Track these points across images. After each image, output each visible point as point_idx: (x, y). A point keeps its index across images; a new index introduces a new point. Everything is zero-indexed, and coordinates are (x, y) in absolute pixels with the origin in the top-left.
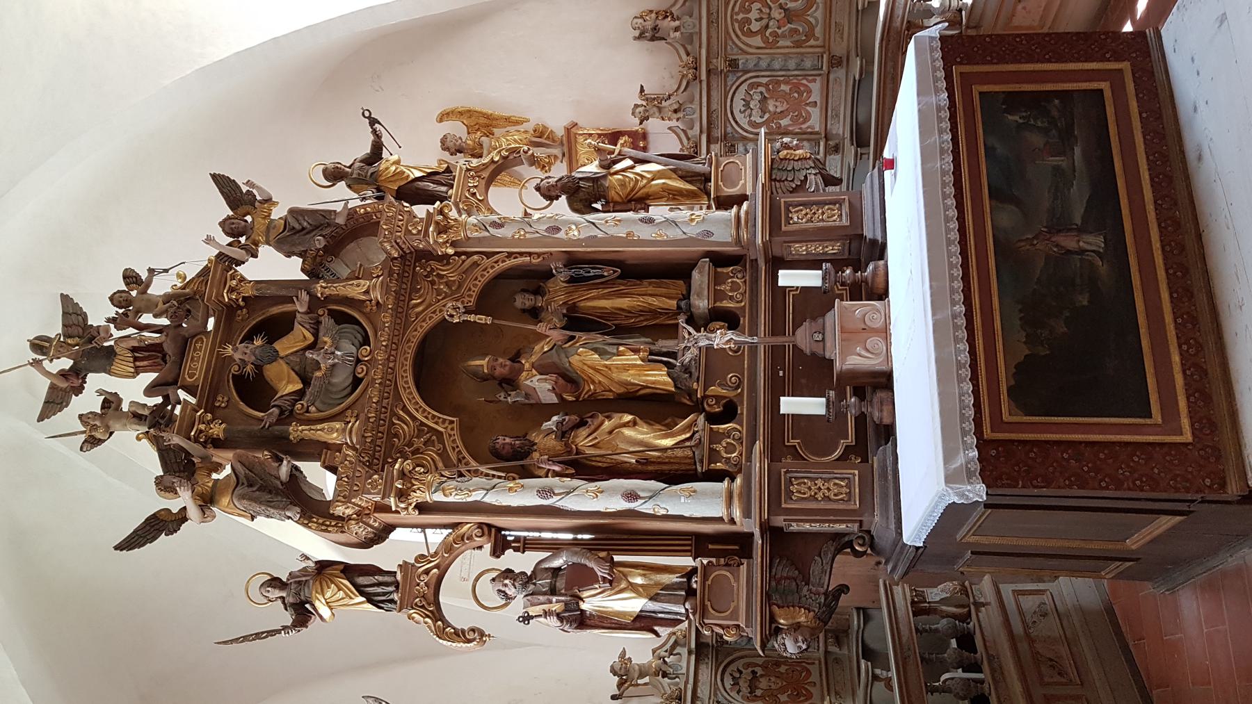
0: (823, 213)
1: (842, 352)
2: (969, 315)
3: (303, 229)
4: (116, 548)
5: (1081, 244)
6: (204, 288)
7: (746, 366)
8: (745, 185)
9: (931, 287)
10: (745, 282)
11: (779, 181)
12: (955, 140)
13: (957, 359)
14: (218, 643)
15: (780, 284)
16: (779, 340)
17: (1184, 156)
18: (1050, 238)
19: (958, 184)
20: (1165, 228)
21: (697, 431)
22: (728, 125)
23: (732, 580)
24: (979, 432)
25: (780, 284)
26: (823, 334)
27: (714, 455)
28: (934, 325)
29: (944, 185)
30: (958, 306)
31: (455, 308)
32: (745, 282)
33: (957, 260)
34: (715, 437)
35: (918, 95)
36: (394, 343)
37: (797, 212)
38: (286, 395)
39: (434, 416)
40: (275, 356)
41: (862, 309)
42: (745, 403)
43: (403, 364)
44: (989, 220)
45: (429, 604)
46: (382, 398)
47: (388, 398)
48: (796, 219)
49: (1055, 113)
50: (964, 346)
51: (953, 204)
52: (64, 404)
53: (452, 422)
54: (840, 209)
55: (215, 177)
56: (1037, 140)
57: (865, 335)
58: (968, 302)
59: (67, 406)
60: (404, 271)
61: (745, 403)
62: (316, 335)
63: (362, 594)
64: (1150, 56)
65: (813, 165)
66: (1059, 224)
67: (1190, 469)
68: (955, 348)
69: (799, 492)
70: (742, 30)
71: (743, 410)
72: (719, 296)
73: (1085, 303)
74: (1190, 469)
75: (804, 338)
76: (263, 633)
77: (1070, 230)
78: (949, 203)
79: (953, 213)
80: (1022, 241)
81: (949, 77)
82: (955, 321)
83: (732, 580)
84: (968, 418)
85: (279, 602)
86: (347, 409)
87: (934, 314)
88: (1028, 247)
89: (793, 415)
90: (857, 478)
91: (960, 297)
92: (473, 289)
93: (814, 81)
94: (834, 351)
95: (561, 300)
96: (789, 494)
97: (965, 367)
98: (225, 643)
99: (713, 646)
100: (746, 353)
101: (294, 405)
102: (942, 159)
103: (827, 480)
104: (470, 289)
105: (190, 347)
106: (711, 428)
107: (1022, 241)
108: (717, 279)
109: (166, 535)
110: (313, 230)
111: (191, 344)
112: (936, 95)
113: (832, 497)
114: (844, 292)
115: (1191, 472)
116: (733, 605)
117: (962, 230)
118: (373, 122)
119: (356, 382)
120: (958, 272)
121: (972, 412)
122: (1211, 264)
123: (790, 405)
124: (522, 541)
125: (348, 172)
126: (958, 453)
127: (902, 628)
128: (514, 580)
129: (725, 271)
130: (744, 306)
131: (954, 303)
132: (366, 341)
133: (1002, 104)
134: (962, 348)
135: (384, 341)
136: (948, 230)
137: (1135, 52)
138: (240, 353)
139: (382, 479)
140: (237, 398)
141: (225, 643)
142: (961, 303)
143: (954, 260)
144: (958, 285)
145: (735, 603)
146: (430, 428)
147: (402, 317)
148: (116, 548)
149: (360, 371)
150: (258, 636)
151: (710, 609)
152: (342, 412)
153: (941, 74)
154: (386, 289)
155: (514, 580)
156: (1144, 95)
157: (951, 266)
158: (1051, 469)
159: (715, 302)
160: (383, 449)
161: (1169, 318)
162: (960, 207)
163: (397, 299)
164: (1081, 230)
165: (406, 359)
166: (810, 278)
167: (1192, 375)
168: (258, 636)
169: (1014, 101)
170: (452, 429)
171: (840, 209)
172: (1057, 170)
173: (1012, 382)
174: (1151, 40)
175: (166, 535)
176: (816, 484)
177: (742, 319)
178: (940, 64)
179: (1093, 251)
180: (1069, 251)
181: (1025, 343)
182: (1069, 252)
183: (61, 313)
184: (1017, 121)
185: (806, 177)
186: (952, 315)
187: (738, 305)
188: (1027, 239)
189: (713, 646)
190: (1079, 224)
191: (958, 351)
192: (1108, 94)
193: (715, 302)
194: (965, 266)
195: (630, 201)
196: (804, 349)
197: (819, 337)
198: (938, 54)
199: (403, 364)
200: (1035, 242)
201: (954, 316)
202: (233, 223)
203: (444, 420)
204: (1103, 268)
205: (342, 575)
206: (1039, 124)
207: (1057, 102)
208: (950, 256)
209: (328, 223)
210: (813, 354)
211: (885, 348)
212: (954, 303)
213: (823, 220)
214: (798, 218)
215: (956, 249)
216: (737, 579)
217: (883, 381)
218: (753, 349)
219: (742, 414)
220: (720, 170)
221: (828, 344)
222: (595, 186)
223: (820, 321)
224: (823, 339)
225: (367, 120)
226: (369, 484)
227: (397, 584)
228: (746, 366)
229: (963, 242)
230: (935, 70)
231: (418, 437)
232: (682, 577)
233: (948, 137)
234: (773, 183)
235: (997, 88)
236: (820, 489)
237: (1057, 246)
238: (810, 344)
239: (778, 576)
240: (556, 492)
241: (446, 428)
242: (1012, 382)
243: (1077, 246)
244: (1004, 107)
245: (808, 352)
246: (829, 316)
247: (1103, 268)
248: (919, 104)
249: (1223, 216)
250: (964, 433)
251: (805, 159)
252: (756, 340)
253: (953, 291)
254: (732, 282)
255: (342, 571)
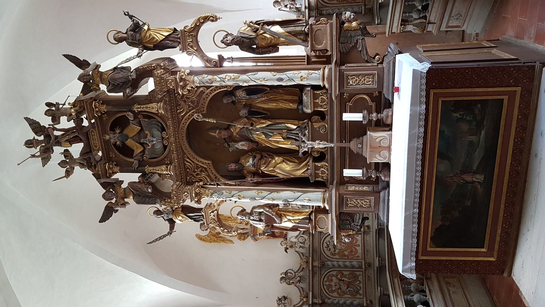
0: (365, 80)
1: (370, 157)
2: (420, 214)
3: (118, 84)
4: (101, 221)
5: (474, 179)
6: (83, 105)
7: (329, 138)
8: (326, 44)
9: (406, 201)
10: (328, 98)
11: (344, 43)
12: (425, 132)
13: (412, 230)
14: (148, 243)
15: (344, 119)
16: (343, 145)
17: (531, 143)
18: (461, 176)
19: (423, 154)
20: (517, 142)
21: (310, 169)
22: (322, 292)
23: (326, 219)
24: (417, 257)
25: (344, 119)
26: (362, 145)
27: (317, 175)
28: (405, 217)
29: (417, 154)
30: (416, 209)
31: (198, 116)
32: (328, 98)
33: (418, 190)
34: (317, 168)
35: (411, 105)
36: (176, 131)
37: (352, 79)
38: (139, 154)
39: (201, 161)
40: (127, 137)
41: (378, 135)
42: (329, 154)
43: (182, 139)
44: (435, 168)
45: (216, 222)
46: (178, 156)
47: (180, 154)
48: (351, 83)
49: (477, 112)
50: (416, 226)
51: (420, 164)
52: (49, 158)
53: (208, 164)
54: (373, 78)
55: (64, 55)
56: (465, 127)
57: (380, 149)
58: (420, 208)
59: (51, 158)
60: (171, 97)
61: (329, 154)
62: (141, 126)
63: (191, 219)
64: (533, 82)
65: (361, 34)
66: (466, 170)
67: (492, 268)
68: (412, 226)
69: (350, 204)
70: (328, 290)
71: (328, 157)
72: (315, 105)
73: (469, 204)
74: (492, 268)
75: (353, 145)
76: (161, 236)
77: (470, 172)
78: (418, 164)
79: (420, 168)
80: (447, 177)
81: (428, 96)
82: (417, 168)
83: (326, 219)
84: (414, 251)
85: (162, 218)
86: (165, 158)
87: (405, 212)
88: (450, 180)
89: (349, 121)
90: (373, 200)
91: (417, 205)
92: (204, 104)
93: (358, 236)
94: (367, 154)
95: (244, 102)
96: (347, 205)
97: (413, 252)
98: (150, 243)
99: (319, 267)
100: (329, 132)
101: (143, 157)
102: (418, 142)
103: (362, 200)
104: (202, 104)
105: (90, 135)
106: (315, 164)
107: (447, 177)
108: (315, 97)
109: (115, 213)
110: (123, 84)
111: (89, 133)
112: (420, 106)
113: (364, 206)
114: (373, 105)
115: (492, 269)
116: (326, 227)
117: (422, 177)
118: (131, 17)
119: (165, 147)
120: (418, 195)
121: (415, 249)
122: (525, 197)
123: (348, 117)
124: (231, 59)
125: (126, 37)
126: (408, 263)
127: (399, 9)
128: (246, 216)
129: (318, 92)
130: (328, 110)
131: (414, 208)
132: (163, 129)
133: (452, 107)
134: (415, 226)
135: (172, 133)
136: (416, 176)
137: (526, 79)
138: (113, 138)
139: (189, 194)
140: (119, 154)
141: (150, 243)
142: (417, 208)
143: (417, 190)
144: (417, 200)
145: (327, 226)
146: (201, 166)
147: (177, 121)
148: (101, 221)
149: (165, 143)
150: (160, 238)
151: (318, 228)
152: (163, 159)
153: (424, 93)
154: (165, 110)
155: (246, 216)
156: (527, 82)
157: (415, 192)
158: (441, 267)
159: (315, 178)
160: (184, 174)
161: (505, 184)
162: (423, 166)
163: (172, 112)
164: (475, 173)
165: (183, 137)
166: (357, 117)
167: (504, 235)
168: (160, 238)
169: (458, 105)
170: (210, 166)
171: (373, 78)
172: (471, 143)
173: (433, 235)
174: (537, 72)
175: (115, 213)
176: (357, 201)
177: (326, 116)
178: (424, 87)
179: (478, 182)
180: (467, 181)
181: (441, 220)
182: (468, 182)
183: (31, 130)
184: (457, 117)
185: (357, 41)
186: (413, 213)
187: (325, 110)
188: (451, 176)
189: (319, 267)
190: (475, 170)
191: (413, 227)
192: (505, 103)
193: (315, 178)
194: (421, 193)
195: (269, 47)
196: (354, 150)
197: (360, 146)
198: (424, 81)
199: (182, 139)
200: (454, 178)
201: (413, 214)
202: (84, 79)
203: (206, 163)
204: (480, 188)
205: (182, 213)
206: (468, 118)
207: (479, 105)
208: (415, 188)
209: (129, 80)
210: (358, 153)
211: (388, 155)
212: (414, 208)
213: (364, 84)
214: (352, 82)
215: (418, 185)
216: (328, 218)
217: (387, 166)
218: (332, 148)
219: (328, 158)
220: (313, 34)
221: (364, 150)
222: (251, 41)
223: (361, 138)
224: (362, 147)
225: (128, 17)
226: (184, 196)
227: (203, 215)
228: (329, 138)
229: (422, 182)
230: (421, 90)
231: (197, 169)
232: (308, 216)
233: (422, 130)
234: (341, 45)
235: (451, 99)
236: (359, 203)
237: (463, 180)
238: (356, 149)
239: (343, 219)
240: (257, 199)
241: (207, 166)
242: (433, 235)
243: (471, 180)
244: (453, 109)
245: (355, 152)
246: (365, 137)
247: (480, 188)
248: (410, 111)
249: (534, 194)
250: (411, 256)
251: (357, 30)
252: (332, 145)
253: (414, 202)
254: (321, 98)
255: (182, 211)
